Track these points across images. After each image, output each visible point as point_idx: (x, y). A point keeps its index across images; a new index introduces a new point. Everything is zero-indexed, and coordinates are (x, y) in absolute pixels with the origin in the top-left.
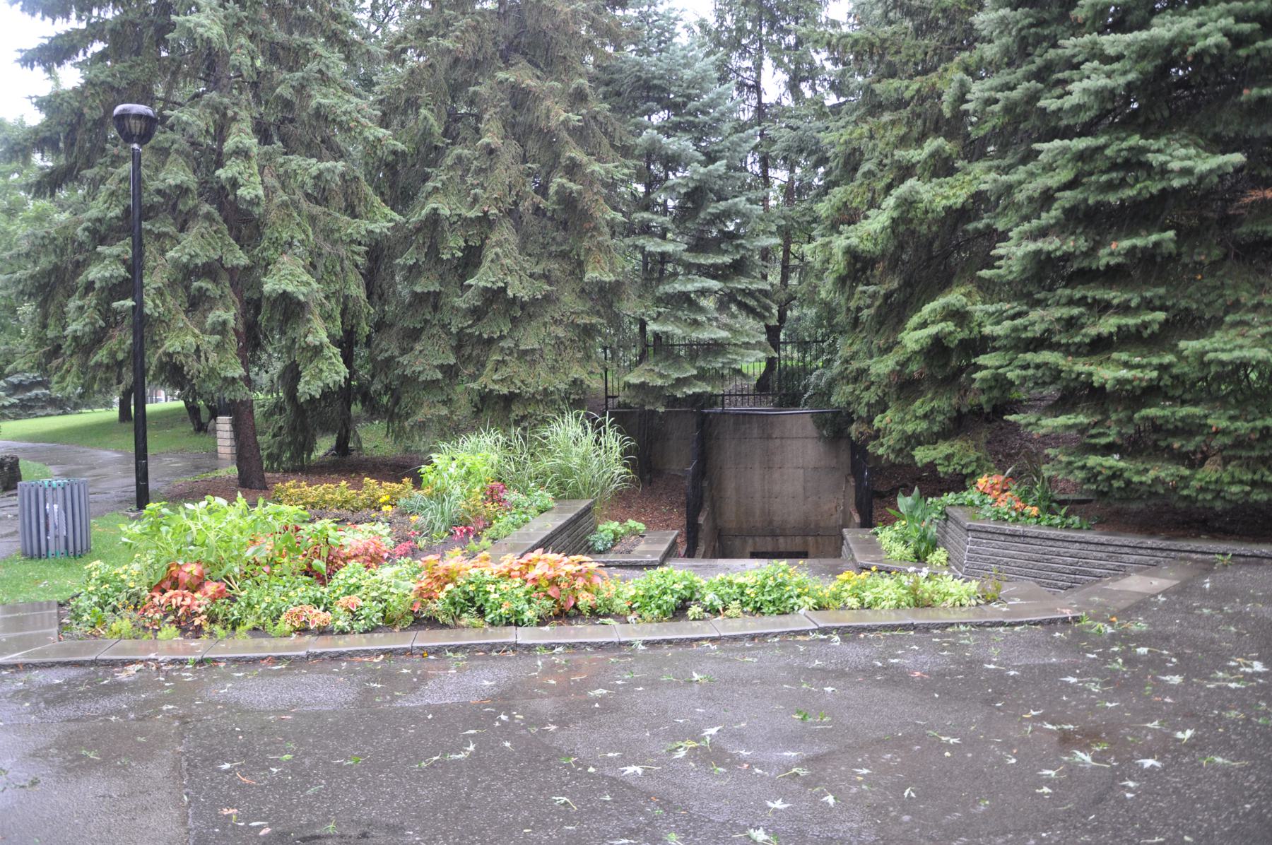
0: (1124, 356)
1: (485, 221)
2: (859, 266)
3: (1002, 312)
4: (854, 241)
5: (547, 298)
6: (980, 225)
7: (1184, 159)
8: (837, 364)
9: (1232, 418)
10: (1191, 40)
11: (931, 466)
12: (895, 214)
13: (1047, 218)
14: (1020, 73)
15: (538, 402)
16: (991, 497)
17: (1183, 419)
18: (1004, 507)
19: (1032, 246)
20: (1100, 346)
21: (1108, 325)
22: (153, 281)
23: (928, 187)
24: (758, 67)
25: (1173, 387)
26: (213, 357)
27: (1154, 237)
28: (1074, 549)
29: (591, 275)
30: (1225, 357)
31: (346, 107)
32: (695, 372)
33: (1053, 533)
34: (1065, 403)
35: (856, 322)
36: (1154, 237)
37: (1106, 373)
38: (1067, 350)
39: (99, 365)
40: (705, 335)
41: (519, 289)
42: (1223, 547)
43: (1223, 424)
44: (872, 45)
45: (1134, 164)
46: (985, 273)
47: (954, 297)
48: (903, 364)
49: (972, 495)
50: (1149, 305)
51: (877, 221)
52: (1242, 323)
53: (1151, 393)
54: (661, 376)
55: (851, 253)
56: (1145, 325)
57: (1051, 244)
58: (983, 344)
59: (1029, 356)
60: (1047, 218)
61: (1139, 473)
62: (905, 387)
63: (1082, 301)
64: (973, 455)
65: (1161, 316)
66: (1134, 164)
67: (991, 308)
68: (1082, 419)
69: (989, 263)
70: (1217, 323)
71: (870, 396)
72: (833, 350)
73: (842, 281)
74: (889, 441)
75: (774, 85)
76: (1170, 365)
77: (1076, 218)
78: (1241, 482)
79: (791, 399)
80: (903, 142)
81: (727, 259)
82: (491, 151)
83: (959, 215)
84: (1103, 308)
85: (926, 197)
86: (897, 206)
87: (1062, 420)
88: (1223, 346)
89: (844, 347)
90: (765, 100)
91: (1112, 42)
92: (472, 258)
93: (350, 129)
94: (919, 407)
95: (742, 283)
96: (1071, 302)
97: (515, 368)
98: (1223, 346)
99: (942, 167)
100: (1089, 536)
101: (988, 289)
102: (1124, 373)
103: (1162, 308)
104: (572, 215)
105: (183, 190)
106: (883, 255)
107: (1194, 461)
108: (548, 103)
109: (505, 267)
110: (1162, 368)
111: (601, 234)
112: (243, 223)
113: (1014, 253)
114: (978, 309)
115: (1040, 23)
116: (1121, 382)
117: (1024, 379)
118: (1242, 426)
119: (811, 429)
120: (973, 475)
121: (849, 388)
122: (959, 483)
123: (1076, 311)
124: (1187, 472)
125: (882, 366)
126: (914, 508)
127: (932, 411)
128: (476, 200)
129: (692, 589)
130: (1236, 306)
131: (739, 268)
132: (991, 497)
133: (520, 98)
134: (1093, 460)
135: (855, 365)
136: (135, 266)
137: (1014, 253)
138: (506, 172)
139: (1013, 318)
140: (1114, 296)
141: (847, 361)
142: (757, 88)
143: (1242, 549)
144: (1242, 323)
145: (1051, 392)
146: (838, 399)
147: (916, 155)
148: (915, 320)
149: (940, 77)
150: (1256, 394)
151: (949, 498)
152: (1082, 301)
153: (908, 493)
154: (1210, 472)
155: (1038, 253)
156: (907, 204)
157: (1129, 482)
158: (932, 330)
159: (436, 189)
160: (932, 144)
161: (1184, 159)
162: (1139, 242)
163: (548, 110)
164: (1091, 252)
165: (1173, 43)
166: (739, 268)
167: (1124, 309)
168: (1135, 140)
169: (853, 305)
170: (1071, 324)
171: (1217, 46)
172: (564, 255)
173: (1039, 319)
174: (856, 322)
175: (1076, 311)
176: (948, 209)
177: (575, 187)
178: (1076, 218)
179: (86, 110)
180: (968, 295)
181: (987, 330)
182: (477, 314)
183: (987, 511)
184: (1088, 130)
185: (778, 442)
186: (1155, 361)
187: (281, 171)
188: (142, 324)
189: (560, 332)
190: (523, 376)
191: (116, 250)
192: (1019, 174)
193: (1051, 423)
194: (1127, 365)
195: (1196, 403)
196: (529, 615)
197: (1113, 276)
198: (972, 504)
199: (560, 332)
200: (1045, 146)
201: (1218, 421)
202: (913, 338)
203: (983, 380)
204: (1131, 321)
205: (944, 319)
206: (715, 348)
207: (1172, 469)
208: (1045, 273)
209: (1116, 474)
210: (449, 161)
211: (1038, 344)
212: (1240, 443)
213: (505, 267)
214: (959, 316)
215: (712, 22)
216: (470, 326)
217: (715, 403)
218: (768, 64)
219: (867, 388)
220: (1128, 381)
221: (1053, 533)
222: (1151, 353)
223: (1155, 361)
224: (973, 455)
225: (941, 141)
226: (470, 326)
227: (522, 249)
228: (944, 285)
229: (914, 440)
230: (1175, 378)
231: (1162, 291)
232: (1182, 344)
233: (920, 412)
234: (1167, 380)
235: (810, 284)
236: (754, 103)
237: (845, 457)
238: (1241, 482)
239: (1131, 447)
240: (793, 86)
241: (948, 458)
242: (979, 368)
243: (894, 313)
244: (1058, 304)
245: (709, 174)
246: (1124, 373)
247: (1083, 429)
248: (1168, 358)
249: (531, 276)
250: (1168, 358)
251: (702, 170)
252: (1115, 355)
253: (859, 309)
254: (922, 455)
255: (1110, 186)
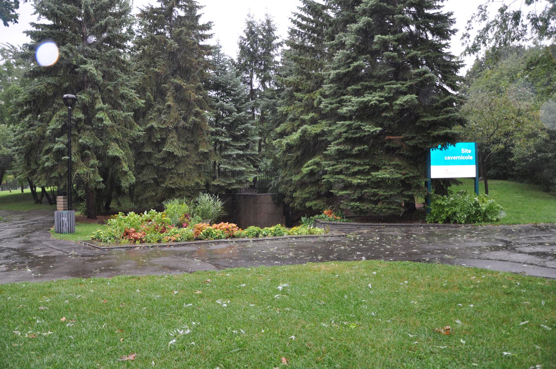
0: (359, 177)
1: (168, 130)
2: (290, 147)
3: (329, 164)
4: (289, 141)
5: (188, 156)
6: (324, 138)
7: (369, 128)
8: (280, 178)
9: (384, 192)
10: (371, 101)
11: (310, 207)
12: (301, 134)
13: (340, 140)
14: (334, 101)
15: (184, 190)
16: (327, 215)
17: (373, 192)
18: (331, 217)
19: (337, 148)
20: (354, 174)
21: (356, 169)
22: (74, 150)
23: (310, 127)
24: (251, 77)
25: (371, 184)
26: (92, 175)
27: (362, 147)
28: (349, 227)
29: (201, 149)
30: (380, 176)
31: (131, 94)
32: (235, 181)
33: (344, 223)
34: (345, 188)
35: (286, 165)
36: (362, 147)
37: (355, 181)
38: (346, 175)
39: (55, 177)
40: (238, 169)
41: (178, 153)
42: (383, 224)
43: (382, 193)
44: (294, 83)
45: (359, 128)
46: (325, 152)
47: (317, 159)
48: (302, 178)
49: (323, 215)
50: (365, 164)
51: (295, 136)
52: (386, 169)
53: (366, 186)
54: (224, 182)
55: (288, 144)
56: (365, 169)
57: (341, 147)
58: (325, 173)
59: (337, 176)
60: (340, 140)
61: (363, 206)
62: (302, 184)
63: (350, 163)
64: (322, 204)
65: (368, 167)
66: (359, 128)
67: (327, 163)
68: (349, 192)
69: (326, 150)
70: (381, 169)
71: (291, 189)
72: (278, 175)
73: (285, 152)
74: (298, 201)
75: (256, 84)
76: (370, 179)
77: (348, 141)
78: (386, 208)
79: (265, 190)
80: (302, 113)
81: (244, 144)
82: (169, 106)
83: (317, 135)
84: (355, 164)
85: (309, 130)
86: (301, 132)
87: (344, 192)
88: (381, 174)
89: (282, 173)
90: (254, 88)
91: (354, 99)
92: (163, 141)
93: (133, 101)
94: (307, 190)
95: (249, 152)
96: (347, 163)
97: (176, 179)
98: (381, 174)
99: (313, 122)
100: (352, 223)
101: (326, 157)
102: (359, 181)
103: (369, 165)
104: (196, 128)
105: (80, 120)
106: (297, 145)
107: (376, 203)
108: (190, 91)
109: (173, 146)
110: (368, 180)
111: (204, 136)
112: (101, 132)
113: (332, 149)
114: (323, 163)
115: (340, 88)
116: (359, 183)
117: (335, 181)
118: (386, 194)
119: (270, 199)
120: (322, 209)
121: (284, 186)
122: (319, 212)
123: (348, 165)
124: (374, 206)
125: (296, 178)
126: (306, 221)
127: (311, 191)
128: (165, 122)
129: (260, 231)
130: (385, 165)
131: (247, 147)
132: (327, 215)
133: (178, 88)
134: (352, 204)
135: (286, 179)
136: (68, 145)
137: (332, 149)
138: (174, 114)
139: (333, 165)
140: (357, 161)
141: (283, 178)
142: (251, 84)
143: (387, 224)
144: (386, 169)
145: (342, 185)
146: (280, 190)
147: (307, 117)
148: (306, 165)
149: (314, 95)
150: (389, 186)
151: (317, 216)
152: (350, 163)
153: (304, 216)
154: (379, 205)
155: (338, 149)
156: (304, 132)
157: (361, 209)
158: (311, 168)
159: (151, 118)
160: (311, 115)
161: (369, 128)
162: (359, 148)
163: (190, 94)
164: (351, 150)
165: (367, 102)
166: (247, 147)
167: (360, 165)
168: (359, 123)
169: (285, 160)
170: (347, 168)
171: (375, 103)
172: (192, 142)
173: (339, 167)
174: (286, 165)
175: (348, 165)
176: (316, 134)
177: (197, 120)
178: (348, 141)
179: (47, 93)
180: (320, 158)
181: (326, 169)
182: (164, 160)
183: (327, 219)
184: (350, 118)
185: (259, 205)
186: (366, 178)
187: (111, 115)
188: (70, 163)
189: (191, 167)
190: (179, 182)
191: (61, 139)
192: (333, 127)
193: (341, 193)
194: (360, 179)
195: (376, 188)
196: (223, 237)
197: (356, 156)
198: (323, 217)
199: (191, 167)
200: (339, 123)
201: (381, 193)
202: (305, 170)
203: (325, 182)
204: (361, 168)
205: (314, 165)
206: (241, 173)
207: (371, 205)
208: (341, 155)
209: (358, 207)
210: (155, 109)
211: (340, 172)
212: (386, 198)
213: (173, 146)
214: (318, 164)
215: (236, 61)
216: (162, 164)
217: (238, 192)
218: (255, 76)
219: (290, 186)
220: (360, 183)
221: (344, 223)
222: (366, 176)
223: (366, 178)
224: (322, 204)
225: (314, 114)
226: (162, 164)
227: (179, 140)
228: (313, 155)
229: (305, 200)
230: (371, 182)
231: (368, 161)
232: (372, 173)
233: (307, 192)
234: (370, 183)
235: (270, 152)
236: (250, 88)
237: (281, 209)
238: (386, 208)
239: (361, 199)
240: (263, 82)
241: (315, 205)
242: (324, 179)
243: (299, 163)
244: (344, 163)
245: (239, 116)
246: (359, 181)
247: (349, 195)
248: (369, 177)
249: (182, 148)
250: (369, 177)
251: (237, 115)
252: (357, 176)
253: (287, 161)
254: (308, 204)
255: (354, 133)
